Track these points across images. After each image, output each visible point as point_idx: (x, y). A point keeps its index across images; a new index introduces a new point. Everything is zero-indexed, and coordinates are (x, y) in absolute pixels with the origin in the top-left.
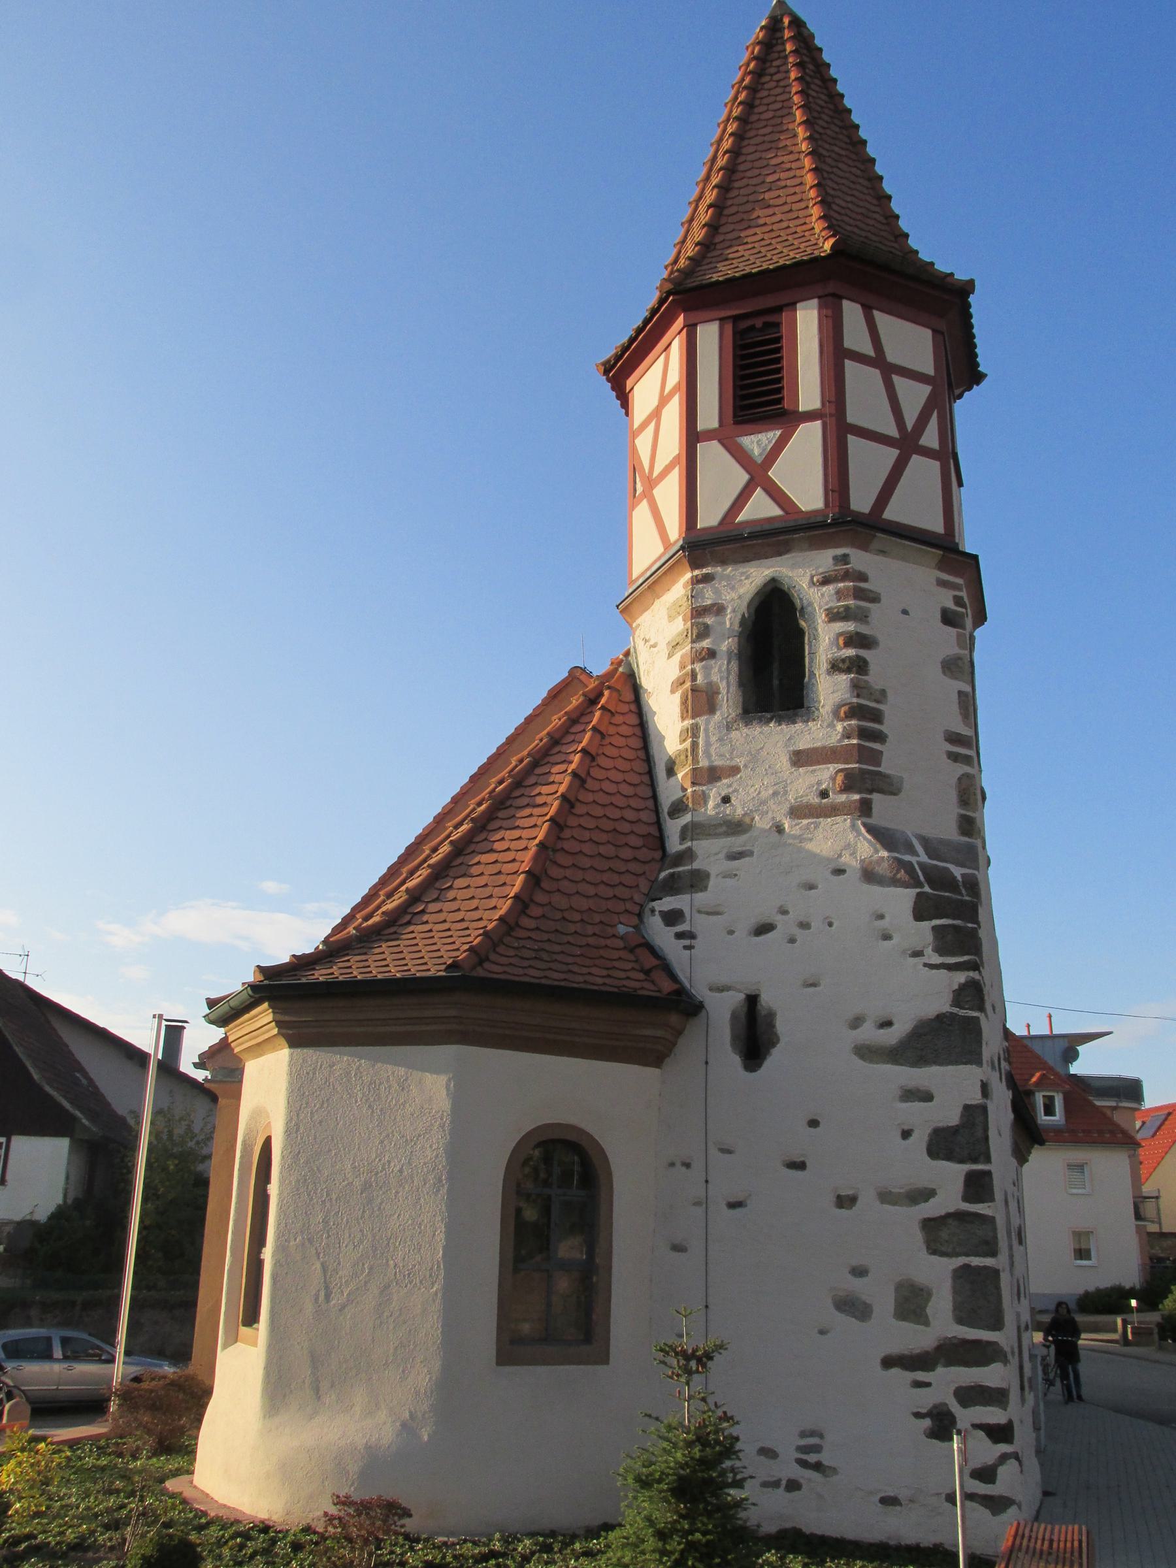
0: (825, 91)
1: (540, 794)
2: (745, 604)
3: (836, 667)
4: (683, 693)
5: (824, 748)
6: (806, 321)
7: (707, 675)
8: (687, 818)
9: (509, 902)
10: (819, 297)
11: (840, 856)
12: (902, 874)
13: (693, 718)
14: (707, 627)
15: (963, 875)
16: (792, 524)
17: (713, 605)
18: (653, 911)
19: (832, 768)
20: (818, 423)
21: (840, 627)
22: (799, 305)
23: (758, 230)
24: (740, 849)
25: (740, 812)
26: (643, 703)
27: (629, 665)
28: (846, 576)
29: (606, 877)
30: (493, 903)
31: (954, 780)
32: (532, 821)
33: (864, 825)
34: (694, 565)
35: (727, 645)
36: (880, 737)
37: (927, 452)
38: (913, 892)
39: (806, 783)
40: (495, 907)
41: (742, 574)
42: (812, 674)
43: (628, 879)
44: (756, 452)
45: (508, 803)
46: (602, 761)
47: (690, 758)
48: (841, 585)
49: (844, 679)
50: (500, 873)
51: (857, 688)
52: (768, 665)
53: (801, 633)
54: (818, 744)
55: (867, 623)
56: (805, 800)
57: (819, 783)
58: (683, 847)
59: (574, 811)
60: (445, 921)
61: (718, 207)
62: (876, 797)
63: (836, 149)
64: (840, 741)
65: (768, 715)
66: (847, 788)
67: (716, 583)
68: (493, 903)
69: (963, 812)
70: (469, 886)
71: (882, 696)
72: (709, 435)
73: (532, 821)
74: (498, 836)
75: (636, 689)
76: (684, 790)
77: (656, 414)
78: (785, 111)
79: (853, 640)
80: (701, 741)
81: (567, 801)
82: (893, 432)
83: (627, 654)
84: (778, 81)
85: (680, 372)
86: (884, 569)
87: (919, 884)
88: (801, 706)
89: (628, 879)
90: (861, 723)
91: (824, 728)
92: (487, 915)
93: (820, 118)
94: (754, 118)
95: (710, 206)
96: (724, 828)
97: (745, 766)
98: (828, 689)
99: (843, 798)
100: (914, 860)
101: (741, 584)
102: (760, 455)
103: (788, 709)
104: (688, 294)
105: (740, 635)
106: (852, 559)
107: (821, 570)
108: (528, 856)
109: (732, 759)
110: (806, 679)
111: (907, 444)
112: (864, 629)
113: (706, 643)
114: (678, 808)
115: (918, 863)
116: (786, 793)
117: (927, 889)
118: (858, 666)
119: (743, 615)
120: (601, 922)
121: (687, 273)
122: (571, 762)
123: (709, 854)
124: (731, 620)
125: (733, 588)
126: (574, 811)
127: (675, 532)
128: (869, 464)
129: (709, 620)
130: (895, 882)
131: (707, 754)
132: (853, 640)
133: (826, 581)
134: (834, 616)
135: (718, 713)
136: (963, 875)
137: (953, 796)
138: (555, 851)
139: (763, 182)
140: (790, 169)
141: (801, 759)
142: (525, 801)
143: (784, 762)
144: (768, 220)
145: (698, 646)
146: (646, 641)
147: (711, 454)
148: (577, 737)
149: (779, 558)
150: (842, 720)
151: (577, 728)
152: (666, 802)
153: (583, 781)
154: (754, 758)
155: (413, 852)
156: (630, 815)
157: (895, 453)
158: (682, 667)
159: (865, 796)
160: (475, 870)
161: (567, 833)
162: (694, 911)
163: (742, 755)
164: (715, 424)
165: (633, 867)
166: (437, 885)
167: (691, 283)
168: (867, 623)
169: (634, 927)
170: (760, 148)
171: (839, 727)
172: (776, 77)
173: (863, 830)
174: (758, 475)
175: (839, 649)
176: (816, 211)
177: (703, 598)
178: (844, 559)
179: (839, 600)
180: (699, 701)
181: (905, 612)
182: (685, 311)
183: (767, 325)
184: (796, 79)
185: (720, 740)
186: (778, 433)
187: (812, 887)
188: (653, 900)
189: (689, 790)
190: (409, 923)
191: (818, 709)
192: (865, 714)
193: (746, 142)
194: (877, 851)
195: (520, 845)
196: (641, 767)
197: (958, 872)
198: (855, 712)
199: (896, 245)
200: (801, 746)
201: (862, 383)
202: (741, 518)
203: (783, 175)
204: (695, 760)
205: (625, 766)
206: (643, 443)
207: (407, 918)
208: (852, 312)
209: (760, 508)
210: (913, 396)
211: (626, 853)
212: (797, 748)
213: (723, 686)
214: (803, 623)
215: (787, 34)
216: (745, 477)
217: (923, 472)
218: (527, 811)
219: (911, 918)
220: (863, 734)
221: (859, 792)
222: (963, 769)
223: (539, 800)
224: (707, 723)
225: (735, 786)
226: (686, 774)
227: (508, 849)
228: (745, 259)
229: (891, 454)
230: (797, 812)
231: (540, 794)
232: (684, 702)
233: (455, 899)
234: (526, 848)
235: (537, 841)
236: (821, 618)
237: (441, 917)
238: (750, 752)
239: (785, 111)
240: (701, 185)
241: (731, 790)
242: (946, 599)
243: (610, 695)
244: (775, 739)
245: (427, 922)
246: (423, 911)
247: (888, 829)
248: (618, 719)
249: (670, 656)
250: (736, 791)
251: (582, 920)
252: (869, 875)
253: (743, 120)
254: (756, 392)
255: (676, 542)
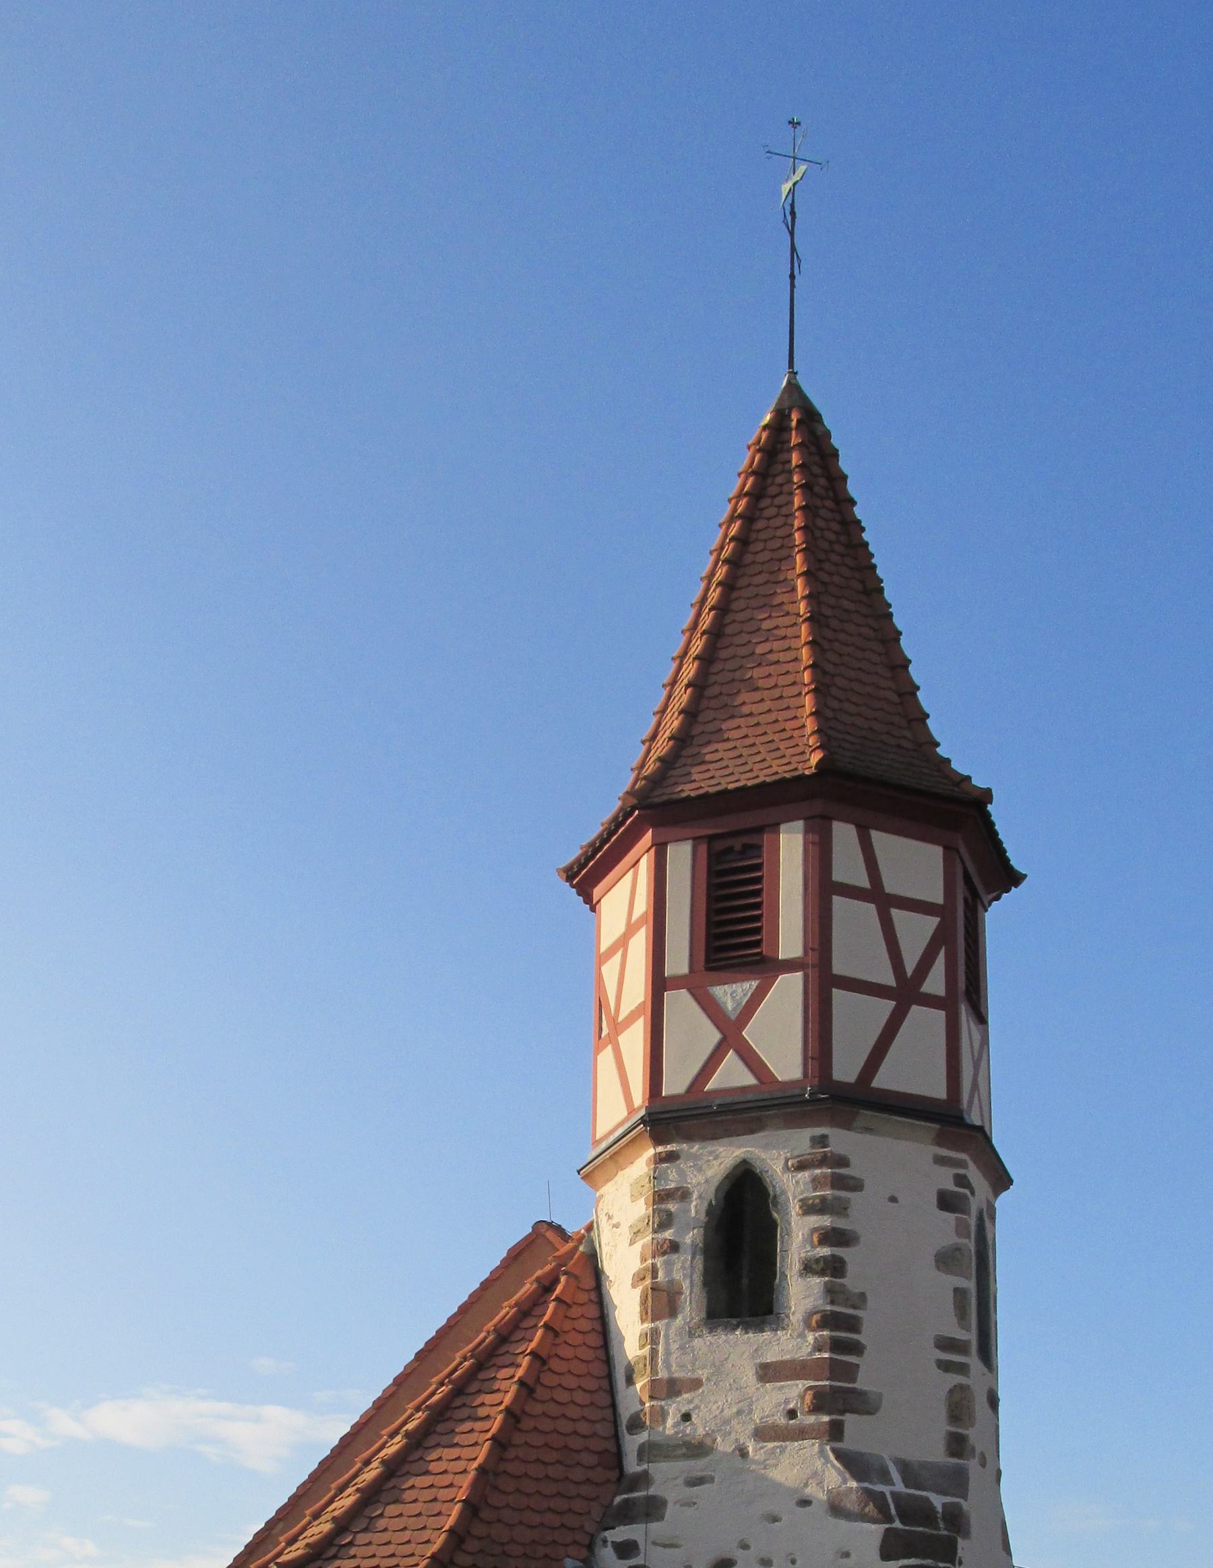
0: (838, 517)
1: (483, 1404)
2: (713, 1189)
3: (809, 1268)
4: (643, 1292)
5: (792, 1361)
6: (790, 846)
7: (669, 1272)
8: (643, 1437)
9: (443, 1536)
10: (805, 819)
11: (806, 1485)
12: (870, 1508)
13: (653, 1321)
14: (670, 1215)
15: (944, 1505)
16: (766, 1096)
17: (677, 1189)
18: (605, 1541)
19: (801, 1385)
20: (799, 974)
21: (815, 1221)
22: (783, 827)
23: (741, 721)
24: (699, 1474)
25: (701, 1431)
26: (604, 1291)
27: (592, 1242)
28: (823, 1161)
29: (553, 1504)
30: (426, 1535)
31: (943, 1394)
32: (472, 1438)
33: (834, 1450)
34: (658, 1140)
35: (691, 1237)
36: (856, 1348)
37: (931, 1001)
38: (881, 1528)
39: (774, 1400)
40: (428, 1541)
41: (711, 1153)
42: (784, 1275)
43: (578, 1505)
44: (730, 1006)
45: (448, 1414)
46: (555, 1364)
47: (648, 1368)
48: (818, 1171)
49: (817, 1282)
50: (435, 1500)
51: (831, 1292)
52: (735, 1260)
53: (773, 1225)
54: (787, 1357)
55: (847, 1216)
56: (770, 1420)
57: (787, 1402)
58: (639, 1469)
59: (519, 1426)
60: (374, 1556)
61: (698, 686)
62: (849, 1419)
63: (846, 604)
64: (810, 1354)
65: (734, 1321)
66: (816, 1409)
67: (681, 1163)
68: (426, 1535)
69: (953, 1429)
70: (401, 1515)
71: (860, 1300)
72: (677, 982)
73: (472, 1438)
74: (434, 1456)
75: (598, 1275)
76: (643, 1403)
77: (622, 943)
78: (784, 553)
79: (832, 1237)
80: (661, 1348)
81: (513, 1416)
82: (889, 980)
83: (590, 1228)
84: (779, 507)
85: (648, 903)
86: (874, 1151)
87: (888, 1519)
88: (770, 1312)
89: (578, 1505)
90: (834, 1334)
91: (793, 1341)
92: (419, 1549)
93: (828, 560)
94: (748, 558)
95: (687, 686)
96: (684, 1450)
97: (708, 1379)
98: (800, 1294)
99: (812, 1419)
100: (886, 1489)
101: (709, 1165)
102: (734, 1009)
103: (756, 1315)
104: (655, 808)
105: (707, 1227)
106: (831, 1140)
107: (796, 1153)
108: (466, 1481)
109: (693, 1371)
110: (777, 1281)
111: (906, 993)
112: (841, 1224)
113: (668, 1234)
114: (636, 1424)
115: (892, 1493)
116: (751, 1411)
117: (897, 1524)
118: (834, 1267)
119: (710, 1204)
120: (546, 1556)
121: (657, 780)
122: (519, 1366)
123: (666, 1479)
124: (696, 1208)
125: (700, 1170)
126: (519, 1426)
127: (639, 1096)
128: (858, 1020)
129: (672, 1207)
130: (864, 1518)
131: (668, 1365)
132: (832, 1237)
133: (801, 1167)
134: (809, 1208)
135: (680, 1317)
136: (944, 1505)
137: (942, 1413)
138: (496, 1474)
139: (753, 653)
140: (784, 638)
141: (769, 1373)
142: (466, 1412)
143: (749, 1376)
144: (756, 709)
145: (660, 1236)
146: (610, 1218)
147: (679, 1003)
148: (528, 1334)
149: (752, 1136)
150: (813, 1330)
151: (527, 1323)
152: (625, 1415)
153: (531, 1391)
154: (718, 1370)
155: (348, 1444)
156: (584, 1428)
157: (887, 1006)
158: (644, 1260)
159: (834, 1417)
160: (408, 1495)
161: (511, 1453)
162: (649, 1542)
163: (704, 1367)
164: (684, 969)
165: (585, 1490)
166: (367, 1512)
167: (658, 797)
168: (847, 1216)
169: (581, 1561)
170: (753, 603)
171: (811, 1338)
172: (777, 501)
173: (832, 1457)
174: (731, 1034)
175: (813, 1247)
176: (808, 702)
177: (667, 1179)
178: (822, 1141)
179: (815, 1190)
180: (660, 1302)
181: (893, 1199)
182: (654, 826)
183: (747, 847)
184: (800, 508)
185: (682, 1348)
186: (755, 984)
187: (775, 1519)
188: (606, 1529)
189: (647, 1405)
190: (335, 1557)
191: (788, 1317)
192: (841, 1324)
193: (735, 595)
194: (845, 1481)
195: (460, 1464)
196: (598, 1369)
197: (938, 1501)
198: (829, 1321)
199: (907, 734)
200: (770, 1358)
201: (854, 922)
202: (709, 1086)
203: (776, 645)
204: (654, 1371)
205: (581, 1368)
206: (610, 971)
207: (333, 1551)
208: (844, 834)
209: (732, 1074)
210: (916, 932)
211: (578, 1474)
212: (764, 1361)
213: (686, 1286)
214: (775, 1215)
215: (795, 439)
216: (716, 1036)
217: (923, 1025)
218: (467, 1426)
219: (877, 1557)
220: (837, 1346)
221: (829, 1413)
222: (955, 1379)
223: (482, 1412)
224: (668, 1327)
225: (696, 1401)
226: (644, 1385)
227: (445, 1472)
228: (722, 770)
229: (887, 1006)
230: (763, 1433)
231: (483, 1404)
232: (644, 1302)
233: (385, 1530)
234: (465, 1471)
235: (475, 1464)
236: (794, 1209)
237: (371, 1550)
238: (713, 1364)
239: (784, 553)
240: (688, 634)
241: (691, 1406)
242: (945, 1179)
243: (567, 1281)
244: (741, 1349)
245: (354, 1557)
246: (351, 1544)
247: (861, 1455)
248: (575, 1312)
249: (632, 1243)
250: (697, 1407)
251: (525, 1554)
252: (836, 1509)
253: (734, 563)
254: (729, 935)
255: (640, 1108)
